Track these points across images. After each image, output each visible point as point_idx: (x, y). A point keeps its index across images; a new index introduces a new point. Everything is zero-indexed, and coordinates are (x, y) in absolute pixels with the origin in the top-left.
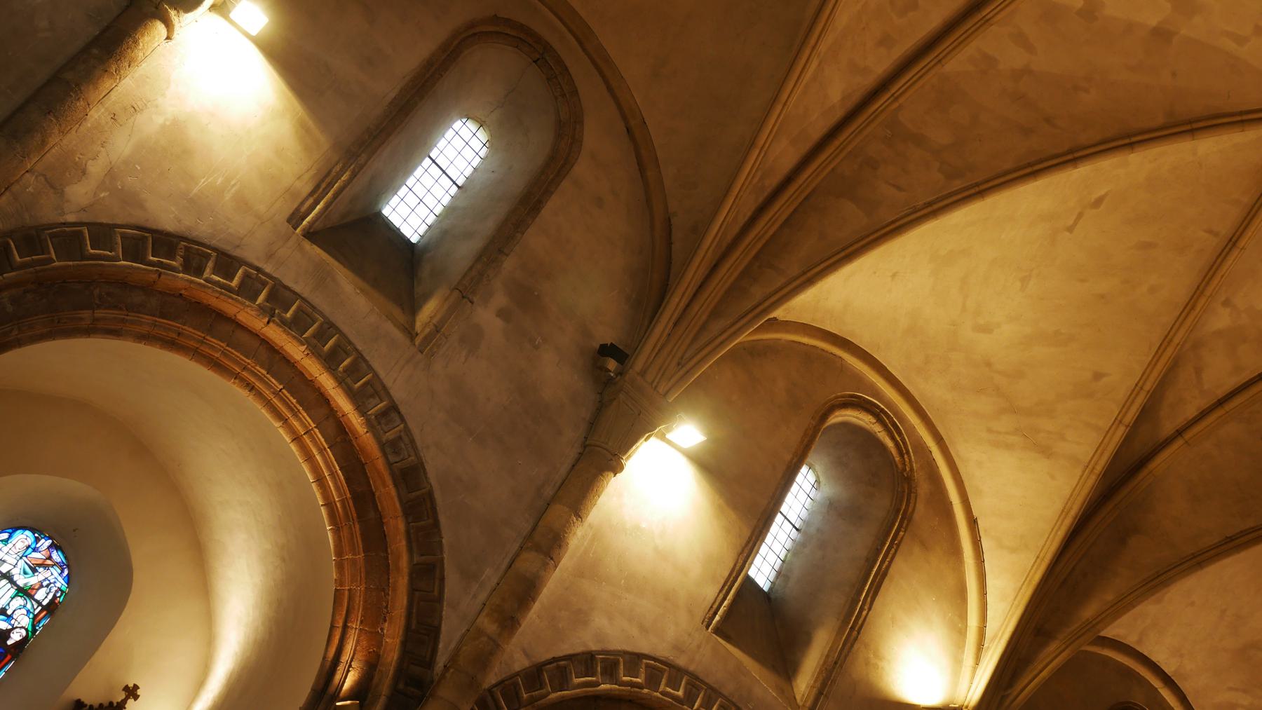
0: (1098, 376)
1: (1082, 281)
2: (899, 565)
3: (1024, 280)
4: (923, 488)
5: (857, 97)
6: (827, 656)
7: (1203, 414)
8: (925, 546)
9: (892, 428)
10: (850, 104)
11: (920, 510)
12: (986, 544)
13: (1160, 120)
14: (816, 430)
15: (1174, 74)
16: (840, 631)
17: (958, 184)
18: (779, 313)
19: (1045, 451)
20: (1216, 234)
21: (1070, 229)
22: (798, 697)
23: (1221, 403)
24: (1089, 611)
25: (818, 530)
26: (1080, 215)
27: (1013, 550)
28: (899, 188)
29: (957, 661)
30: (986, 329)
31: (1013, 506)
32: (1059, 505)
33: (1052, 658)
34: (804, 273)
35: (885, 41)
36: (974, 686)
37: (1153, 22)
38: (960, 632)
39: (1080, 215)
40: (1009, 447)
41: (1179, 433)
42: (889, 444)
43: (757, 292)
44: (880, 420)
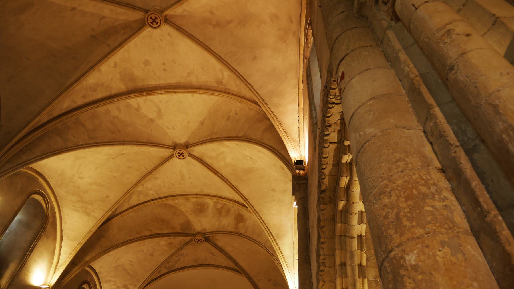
0: (107, 197)
1: (111, 172)
2: (40, 243)
3: (96, 168)
4: (51, 220)
5: (70, 108)
6: (14, 272)
7: (127, 210)
8: (47, 237)
9: (46, 201)
10: (67, 110)
11: (49, 226)
12: (64, 237)
13: (145, 141)
14: (26, 200)
15: (151, 131)
16: (19, 264)
17: (92, 141)
18: (30, 166)
19: (88, 214)
20: (147, 169)
21: (113, 159)
22: (2, 286)
23: (132, 207)
24: (88, 258)
25: (14, 229)
26: (117, 156)
27: (72, 240)
28: (74, 137)
29: (49, 272)
30: (81, 178)
31: (74, 227)
32: (88, 230)
33: (76, 271)
34: (41, 155)
35: (84, 97)
36: (53, 280)
37: (151, 117)
38: (51, 263)
39: (117, 156)
40: (78, 211)
41: (121, 213)
42: (44, 206)
43: (24, 158)
44: (44, 199)
